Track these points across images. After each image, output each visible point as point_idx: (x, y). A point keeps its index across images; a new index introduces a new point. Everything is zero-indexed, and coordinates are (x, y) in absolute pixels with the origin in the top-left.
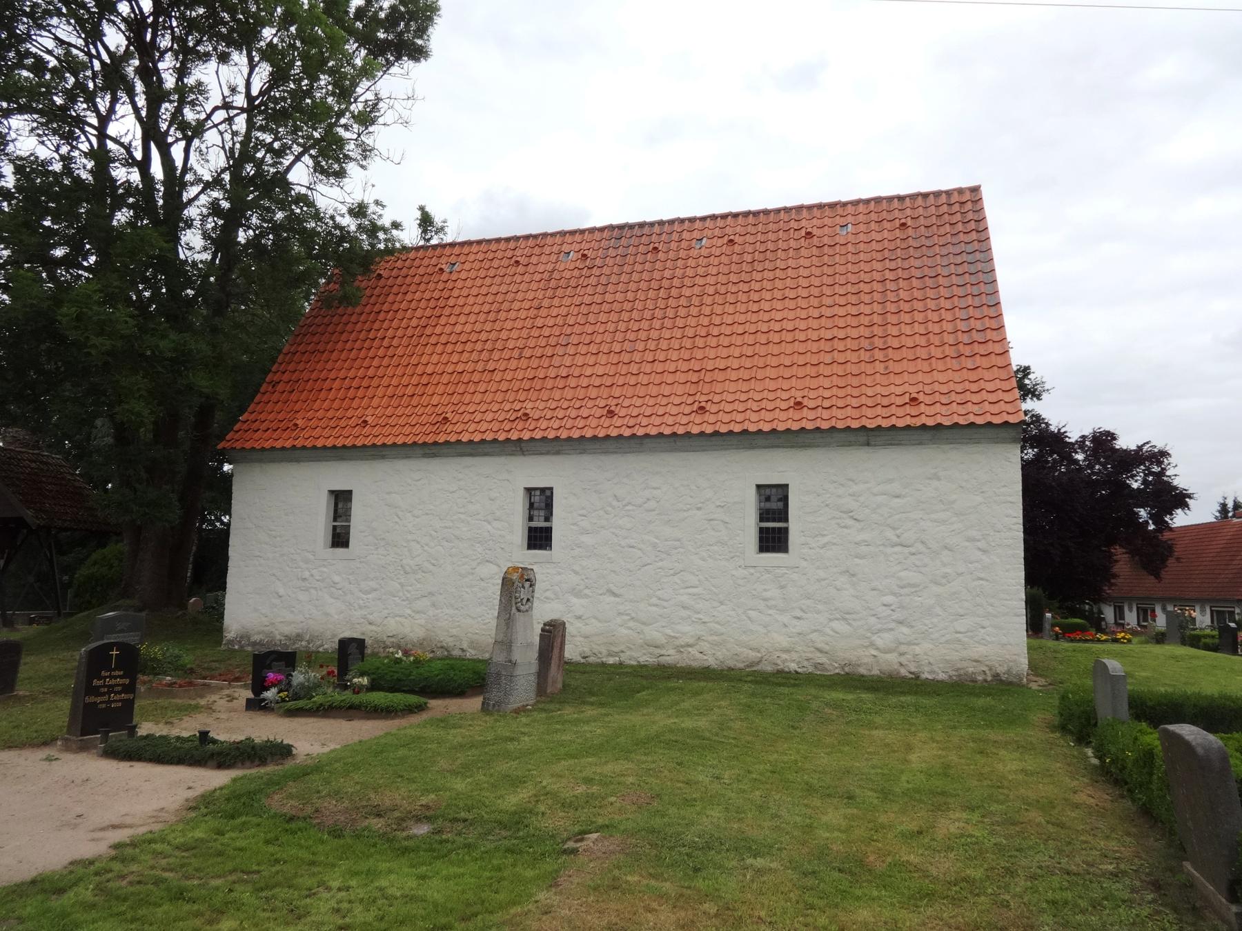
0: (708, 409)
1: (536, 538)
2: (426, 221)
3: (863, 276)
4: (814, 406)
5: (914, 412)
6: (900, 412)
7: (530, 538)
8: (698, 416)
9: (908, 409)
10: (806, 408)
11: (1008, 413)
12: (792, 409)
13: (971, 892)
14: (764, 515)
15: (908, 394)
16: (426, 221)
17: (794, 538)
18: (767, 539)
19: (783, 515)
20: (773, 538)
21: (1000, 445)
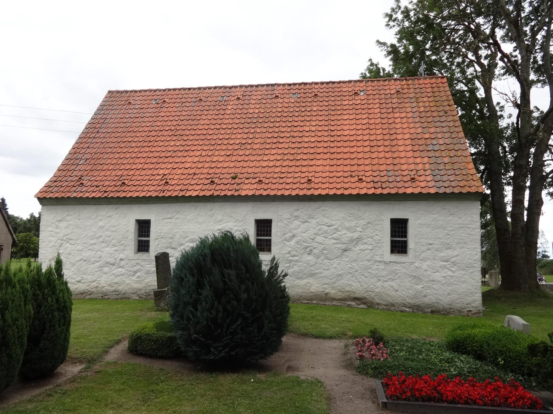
0: (263, 182)
1: (402, 247)
2: (396, 34)
3: (331, 103)
4: (376, 181)
5: (309, 186)
6: (353, 186)
7: (139, 246)
8: (259, 185)
9: (305, 185)
10: (313, 183)
11: (445, 187)
12: (256, 184)
13: (431, 358)
14: (393, 234)
15: (307, 177)
16: (396, 34)
17: (411, 245)
18: (142, 245)
19: (404, 233)
20: (145, 245)
21: (188, 203)
